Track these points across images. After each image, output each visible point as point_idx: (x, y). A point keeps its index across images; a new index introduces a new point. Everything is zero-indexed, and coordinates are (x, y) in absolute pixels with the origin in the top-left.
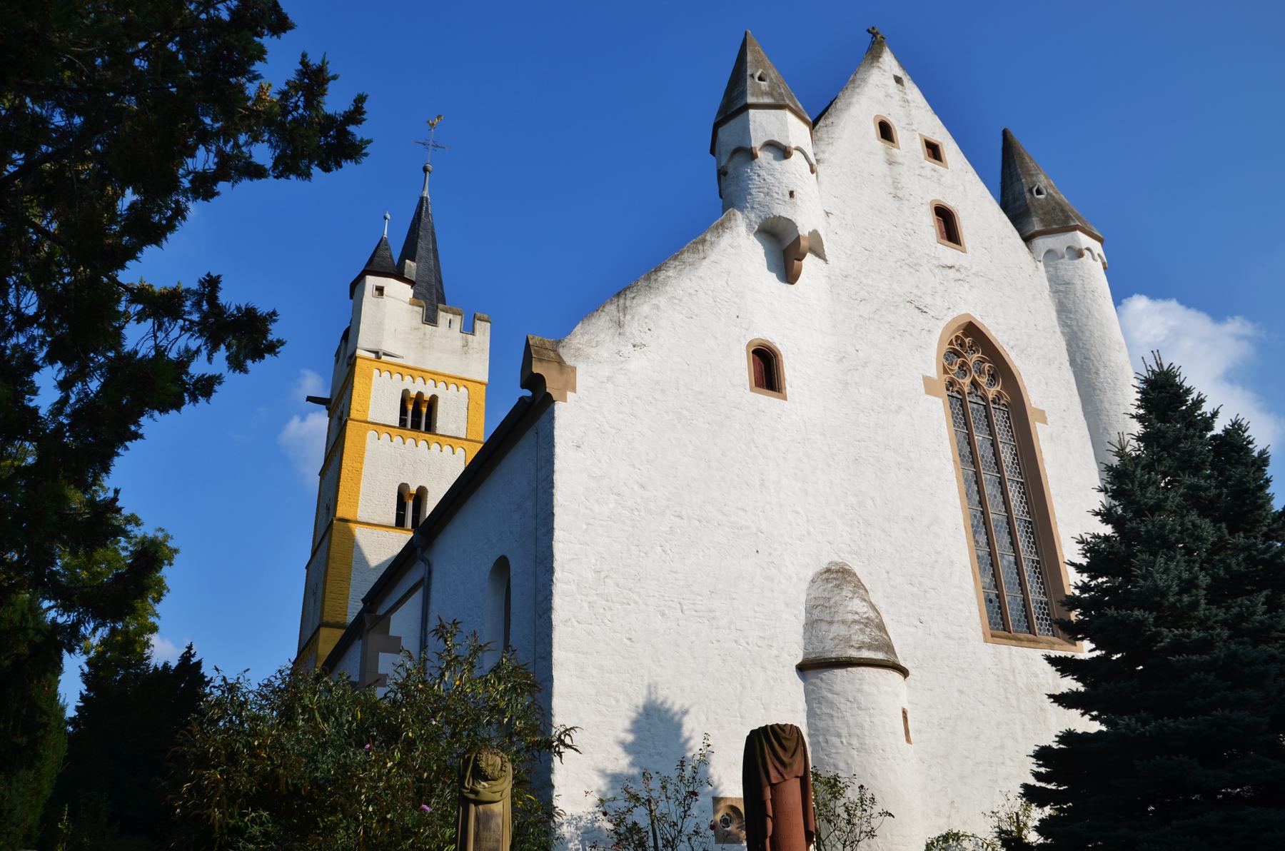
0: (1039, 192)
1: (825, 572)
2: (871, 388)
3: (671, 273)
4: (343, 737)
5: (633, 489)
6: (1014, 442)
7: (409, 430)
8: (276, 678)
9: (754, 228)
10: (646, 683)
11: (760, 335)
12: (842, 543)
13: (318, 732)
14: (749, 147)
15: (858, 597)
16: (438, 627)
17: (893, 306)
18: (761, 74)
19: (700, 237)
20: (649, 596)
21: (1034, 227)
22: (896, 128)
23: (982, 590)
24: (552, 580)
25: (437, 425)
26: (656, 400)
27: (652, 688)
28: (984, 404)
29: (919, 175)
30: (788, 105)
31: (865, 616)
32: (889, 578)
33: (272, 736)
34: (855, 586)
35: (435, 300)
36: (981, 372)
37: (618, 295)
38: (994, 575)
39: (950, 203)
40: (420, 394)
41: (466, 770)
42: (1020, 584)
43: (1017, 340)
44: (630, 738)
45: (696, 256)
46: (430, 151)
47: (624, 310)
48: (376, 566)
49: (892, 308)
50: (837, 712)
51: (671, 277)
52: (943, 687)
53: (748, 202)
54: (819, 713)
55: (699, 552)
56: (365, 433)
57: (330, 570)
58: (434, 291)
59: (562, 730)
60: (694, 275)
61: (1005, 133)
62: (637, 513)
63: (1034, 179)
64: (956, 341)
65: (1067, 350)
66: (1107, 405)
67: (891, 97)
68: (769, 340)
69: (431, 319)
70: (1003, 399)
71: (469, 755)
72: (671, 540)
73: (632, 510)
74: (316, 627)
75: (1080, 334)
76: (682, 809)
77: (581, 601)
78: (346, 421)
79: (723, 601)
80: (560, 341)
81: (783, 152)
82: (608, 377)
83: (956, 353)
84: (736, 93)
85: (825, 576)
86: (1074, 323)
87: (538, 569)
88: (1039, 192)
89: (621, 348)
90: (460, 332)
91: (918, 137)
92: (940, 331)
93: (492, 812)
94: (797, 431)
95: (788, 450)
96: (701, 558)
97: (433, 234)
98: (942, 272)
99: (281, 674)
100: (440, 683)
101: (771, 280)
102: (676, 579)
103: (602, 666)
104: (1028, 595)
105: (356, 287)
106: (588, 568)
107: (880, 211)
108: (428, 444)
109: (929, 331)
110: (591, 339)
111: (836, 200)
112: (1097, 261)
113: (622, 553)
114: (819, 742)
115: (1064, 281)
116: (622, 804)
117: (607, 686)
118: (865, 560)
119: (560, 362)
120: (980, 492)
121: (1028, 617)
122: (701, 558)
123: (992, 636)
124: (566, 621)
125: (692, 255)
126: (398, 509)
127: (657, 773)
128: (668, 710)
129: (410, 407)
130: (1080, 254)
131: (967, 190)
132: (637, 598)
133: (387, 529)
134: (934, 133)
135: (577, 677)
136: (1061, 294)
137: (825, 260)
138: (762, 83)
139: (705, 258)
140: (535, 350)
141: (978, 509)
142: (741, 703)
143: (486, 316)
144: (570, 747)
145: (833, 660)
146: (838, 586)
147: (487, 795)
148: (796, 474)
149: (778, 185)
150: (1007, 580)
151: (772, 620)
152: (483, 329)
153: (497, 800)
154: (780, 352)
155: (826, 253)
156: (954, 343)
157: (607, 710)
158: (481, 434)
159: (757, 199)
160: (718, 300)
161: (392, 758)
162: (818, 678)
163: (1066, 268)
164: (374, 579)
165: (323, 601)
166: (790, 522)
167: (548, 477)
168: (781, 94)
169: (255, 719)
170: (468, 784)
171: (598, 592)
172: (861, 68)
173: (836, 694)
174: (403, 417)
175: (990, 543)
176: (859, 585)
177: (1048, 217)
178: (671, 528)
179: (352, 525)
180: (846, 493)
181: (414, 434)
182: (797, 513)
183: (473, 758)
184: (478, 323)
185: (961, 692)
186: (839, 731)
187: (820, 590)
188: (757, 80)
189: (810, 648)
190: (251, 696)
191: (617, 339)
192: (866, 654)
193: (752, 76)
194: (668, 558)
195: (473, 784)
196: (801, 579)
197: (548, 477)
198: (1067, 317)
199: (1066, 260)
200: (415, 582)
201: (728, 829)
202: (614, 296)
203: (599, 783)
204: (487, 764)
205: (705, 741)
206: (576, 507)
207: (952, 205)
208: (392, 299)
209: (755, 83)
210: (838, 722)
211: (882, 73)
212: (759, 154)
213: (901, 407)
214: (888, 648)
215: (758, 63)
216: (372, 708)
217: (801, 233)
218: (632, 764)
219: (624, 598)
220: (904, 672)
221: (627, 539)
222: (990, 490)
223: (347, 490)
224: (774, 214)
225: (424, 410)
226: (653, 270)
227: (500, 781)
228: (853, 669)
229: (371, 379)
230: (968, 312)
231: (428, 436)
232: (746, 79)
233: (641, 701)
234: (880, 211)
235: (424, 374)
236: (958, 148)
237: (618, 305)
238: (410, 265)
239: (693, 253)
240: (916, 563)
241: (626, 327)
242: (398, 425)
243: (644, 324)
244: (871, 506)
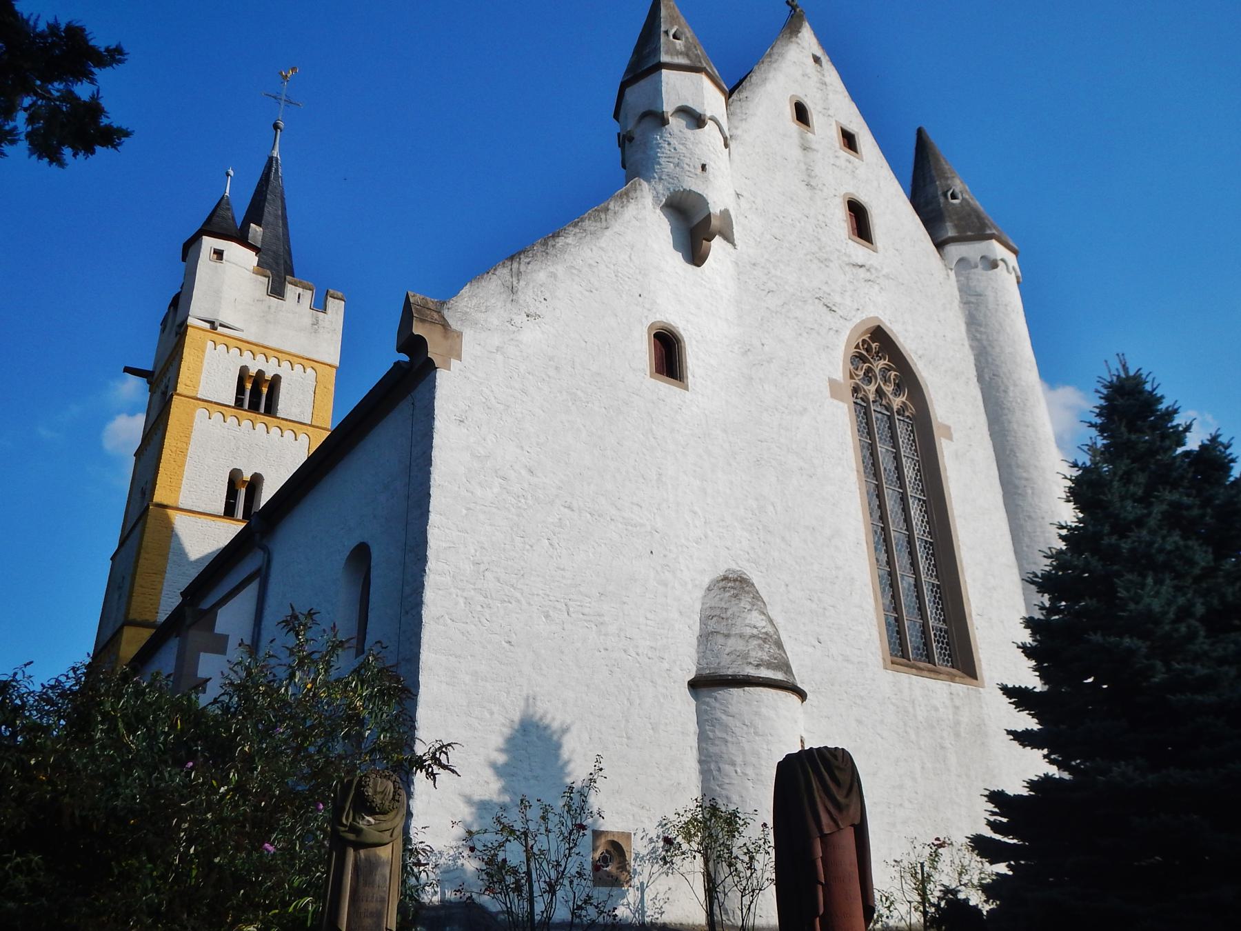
0: (954, 196)
1: (722, 580)
2: (776, 386)
3: (570, 240)
4: (157, 753)
5: (520, 473)
6: (917, 456)
7: (245, 410)
8: (68, 678)
9: (661, 201)
10: (524, 693)
11: (663, 317)
12: (741, 550)
13: (120, 746)
14: (660, 111)
15: (756, 610)
16: (289, 618)
17: (801, 301)
18: (675, 32)
19: (602, 205)
21: (948, 232)
22: (812, 111)
23: (882, 613)
25: (279, 407)
26: (549, 377)
27: (531, 700)
28: (889, 414)
29: (833, 165)
30: (705, 68)
31: (763, 631)
32: (789, 592)
33: (56, 751)
34: (753, 598)
35: (283, 272)
36: (886, 381)
37: (512, 258)
38: (893, 597)
39: (863, 198)
40: (260, 373)
41: (344, 800)
42: (919, 609)
43: (925, 349)
44: (501, 759)
45: (598, 224)
46: (282, 107)
47: (518, 276)
48: (198, 559)
49: (800, 303)
51: (570, 244)
52: (841, 716)
53: (656, 173)
54: (712, 736)
55: (589, 548)
56: (194, 410)
57: (142, 561)
58: (282, 262)
59: (437, 746)
60: (595, 245)
61: (920, 132)
62: (523, 501)
63: (949, 182)
64: (863, 345)
65: (976, 365)
66: (1015, 426)
67: (809, 77)
68: (672, 324)
69: (277, 291)
70: (908, 411)
71: (349, 778)
72: (559, 533)
73: (518, 497)
74: (118, 625)
75: (989, 349)
76: (567, 845)
77: (457, 596)
78: (172, 396)
79: (612, 605)
80: (444, 303)
81: (697, 120)
82: (498, 347)
83: (863, 359)
84: (647, 51)
85: (723, 583)
86: (984, 337)
87: (406, 557)
88: (954, 196)
89: (513, 317)
90: (310, 308)
91: (834, 123)
92: (848, 333)
93: (378, 858)
94: (698, 425)
95: (688, 444)
96: (591, 555)
97: (283, 200)
98: (852, 270)
99: (75, 672)
100: (289, 684)
101: (676, 260)
102: (563, 577)
103: (476, 672)
104: (928, 621)
105: (190, 248)
106: (466, 558)
107: (792, 199)
108: (267, 428)
109: (837, 331)
110: (479, 304)
111: (747, 181)
112: (1011, 274)
113: (505, 544)
114: (710, 771)
115: (976, 292)
116: (491, 838)
117: (481, 696)
118: (764, 570)
119: (445, 326)
120: (882, 506)
121: (927, 644)
122: (591, 555)
123: (893, 663)
124: (438, 618)
125: (594, 224)
126: (228, 497)
127: (539, 800)
128: (546, 728)
129: (249, 386)
130: (994, 265)
131: (881, 185)
133: (214, 519)
134: (851, 122)
136: (972, 305)
137: (734, 245)
138: (677, 41)
140: (415, 308)
141: (879, 524)
142: (627, 721)
143: (340, 294)
144: (445, 767)
145: (730, 678)
146: (735, 596)
147: (373, 835)
148: (695, 471)
149: (690, 156)
150: (907, 604)
151: (664, 629)
152: (336, 308)
153: (387, 841)
154: (683, 339)
155: (735, 237)
156: (861, 347)
157: (479, 724)
158: (328, 420)
159: (666, 170)
160: (620, 275)
161: (225, 780)
162: (710, 697)
163: (978, 279)
164: (194, 573)
165: (130, 596)
166: (687, 522)
167: (424, 453)
168: (697, 56)
169: (35, 729)
170: (347, 819)
171: (476, 587)
172: (778, 42)
174: (239, 396)
175: (890, 562)
176: (757, 597)
177: (963, 223)
178: (560, 519)
179: (170, 512)
180: (747, 496)
181: (252, 415)
182: (695, 513)
183: (355, 782)
184: (330, 301)
185: (859, 722)
186: (733, 758)
187: (717, 599)
188: (671, 37)
189: (704, 662)
190: (31, 700)
191: (509, 305)
192: (765, 673)
193: (666, 32)
194: (556, 553)
195: (354, 819)
196: (696, 586)
197: (424, 453)
198: (977, 331)
199: (979, 270)
200: (249, 573)
201: (607, 869)
202: (507, 259)
203: (465, 813)
204: (375, 792)
205: (597, 764)
206: (457, 489)
207: (866, 201)
208: (234, 265)
209: (669, 41)
210: (732, 749)
212: (670, 119)
213: (805, 409)
214: (785, 667)
215: (673, 20)
216: (196, 717)
217: (711, 211)
218: (504, 790)
219: (506, 595)
220: (802, 695)
221: (512, 529)
222: (892, 504)
223: (169, 473)
224: (684, 187)
225: (265, 390)
226: (551, 235)
227: (392, 815)
228: (751, 688)
229: (204, 352)
230: (876, 315)
231: (267, 419)
232: (660, 35)
233: (517, 717)
234: (792, 199)
235: (267, 351)
236: (874, 140)
237: (511, 269)
238: (256, 230)
239: (596, 221)
240: (816, 577)
241: (519, 293)
242: (233, 405)
243: (539, 292)
244: (771, 512)
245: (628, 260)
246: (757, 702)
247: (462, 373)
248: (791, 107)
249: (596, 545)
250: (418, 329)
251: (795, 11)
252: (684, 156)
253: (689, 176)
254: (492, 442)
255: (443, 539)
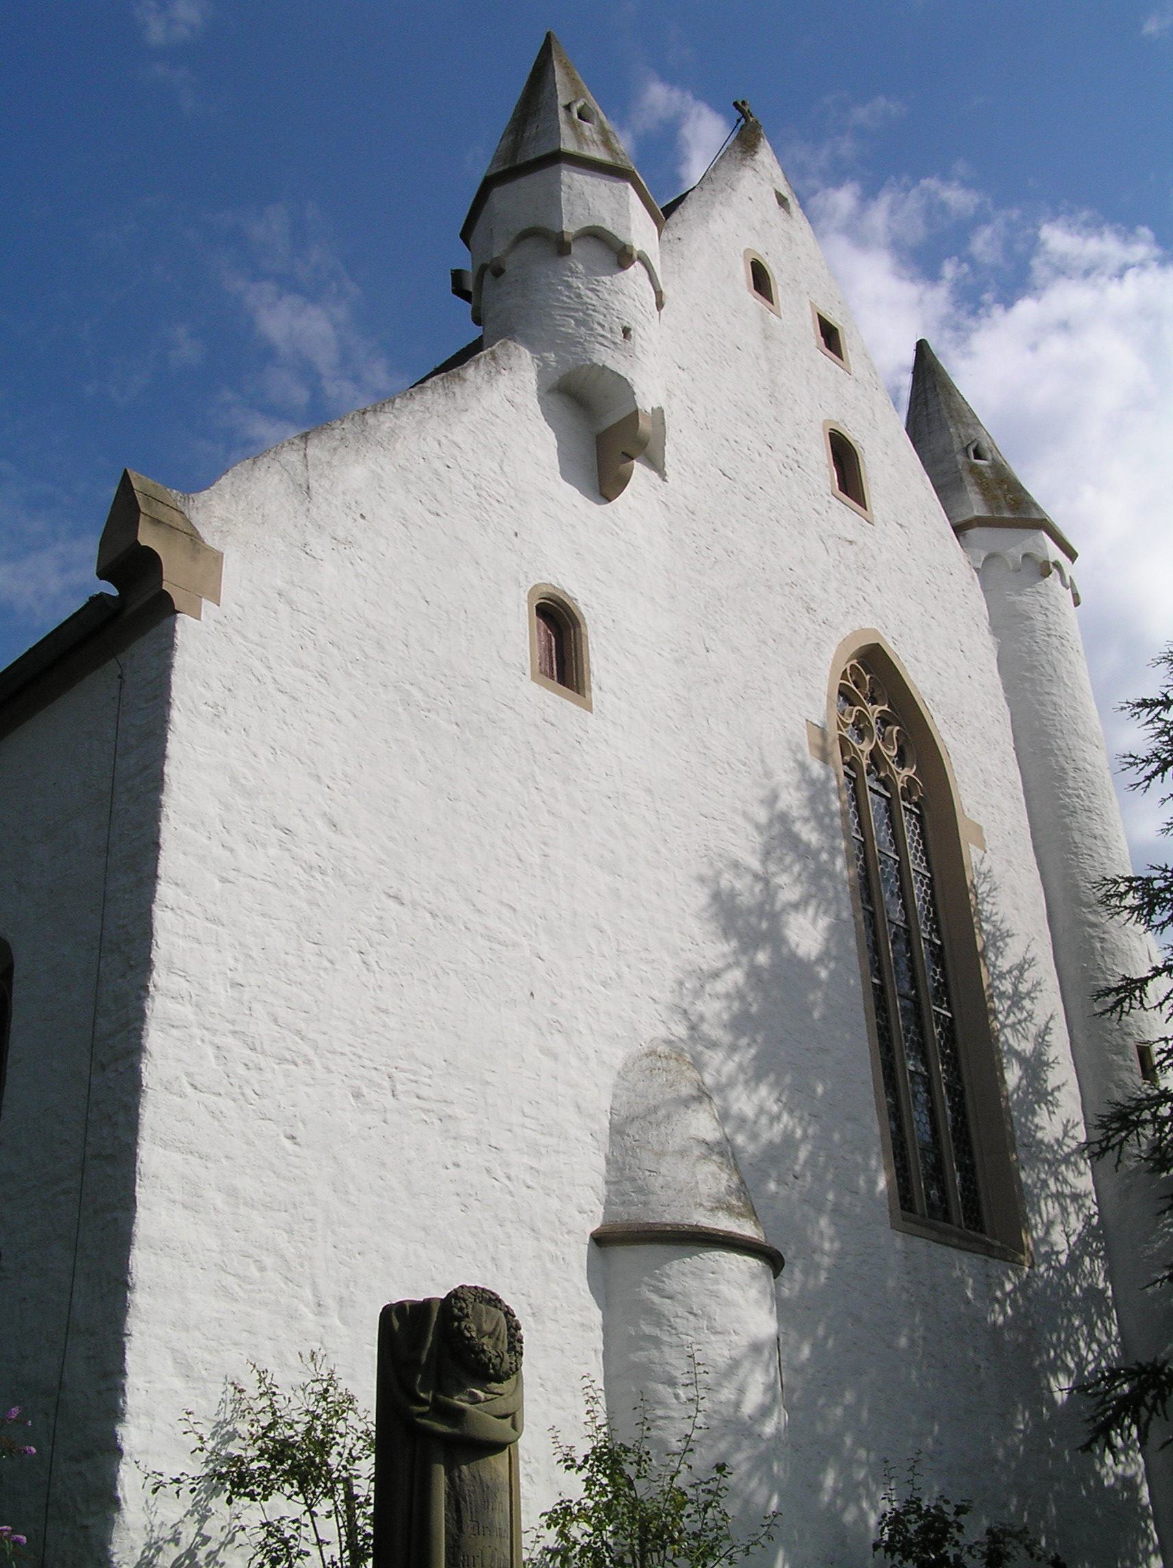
1: (647, 1055)
20: (334, 1052)
24: (146, 988)
39: (852, 435)
50: (671, 1334)
81: (622, 256)
92: (834, 649)
103: (235, 1189)
119: (194, 538)
132: (311, 1053)
135: (185, 1207)
137: (663, 475)
139: (466, 410)
145: (668, 1228)
157: (240, 1286)
171: (237, 1028)
173: (668, 1298)
188: (576, 116)
193: (568, 108)
211: (759, 180)
217: (639, 406)
221: (299, 927)
245: (498, 470)
246: (713, 1273)
247: (219, 627)
248: (746, 268)
249: (439, 972)
250: (147, 537)
251: (747, 120)
252: (594, 311)
253: (603, 345)
254: (269, 761)
255: (181, 932)
